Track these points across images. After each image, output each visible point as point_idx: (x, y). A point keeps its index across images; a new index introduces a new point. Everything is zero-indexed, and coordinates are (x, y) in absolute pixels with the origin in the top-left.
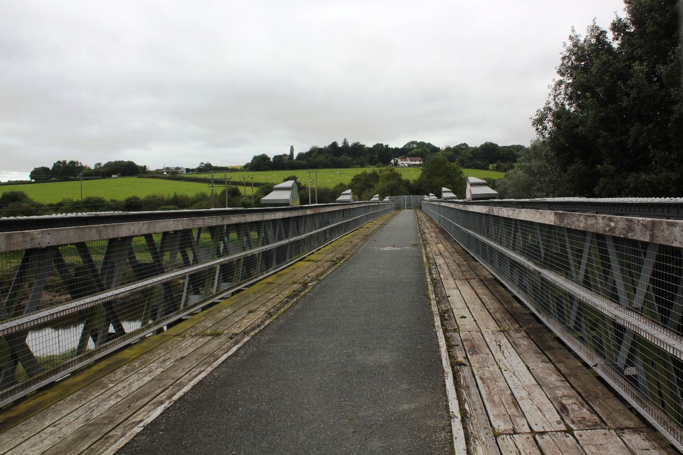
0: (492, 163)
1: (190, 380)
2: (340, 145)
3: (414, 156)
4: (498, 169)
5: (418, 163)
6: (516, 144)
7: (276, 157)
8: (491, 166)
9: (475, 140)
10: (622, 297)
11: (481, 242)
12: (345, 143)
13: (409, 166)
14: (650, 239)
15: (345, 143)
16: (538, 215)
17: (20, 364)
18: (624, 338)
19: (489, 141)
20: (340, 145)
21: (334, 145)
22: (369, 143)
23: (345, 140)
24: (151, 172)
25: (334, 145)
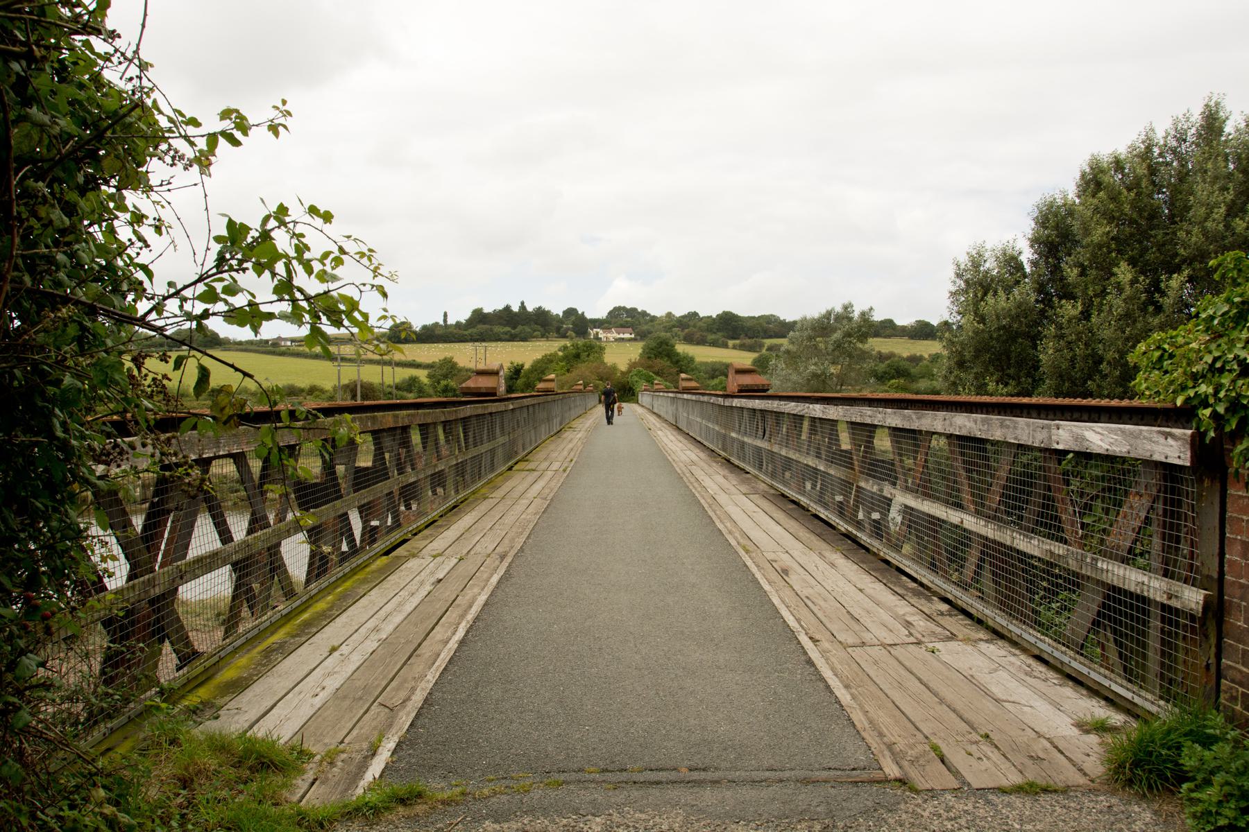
0: (733, 338)
1: (462, 616)
2: (515, 308)
3: (623, 326)
4: (742, 347)
5: (627, 336)
6: (767, 313)
7: (425, 327)
8: (731, 343)
9: (710, 309)
10: (966, 497)
11: (938, 499)
12: (523, 306)
13: (617, 340)
14: (633, 365)
15: (523, 306)
16: (909, 418)
17: (167, 643)
18: (1152, 615)
19: (727, 310)
20: (515, 309)
21: (507, 308)
22: (557, 308)
23: (522, 303)
24: (903, 329)
25: (507, 308)
